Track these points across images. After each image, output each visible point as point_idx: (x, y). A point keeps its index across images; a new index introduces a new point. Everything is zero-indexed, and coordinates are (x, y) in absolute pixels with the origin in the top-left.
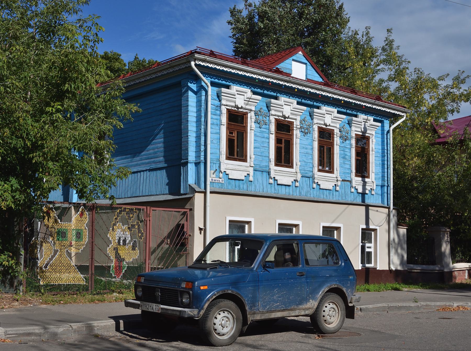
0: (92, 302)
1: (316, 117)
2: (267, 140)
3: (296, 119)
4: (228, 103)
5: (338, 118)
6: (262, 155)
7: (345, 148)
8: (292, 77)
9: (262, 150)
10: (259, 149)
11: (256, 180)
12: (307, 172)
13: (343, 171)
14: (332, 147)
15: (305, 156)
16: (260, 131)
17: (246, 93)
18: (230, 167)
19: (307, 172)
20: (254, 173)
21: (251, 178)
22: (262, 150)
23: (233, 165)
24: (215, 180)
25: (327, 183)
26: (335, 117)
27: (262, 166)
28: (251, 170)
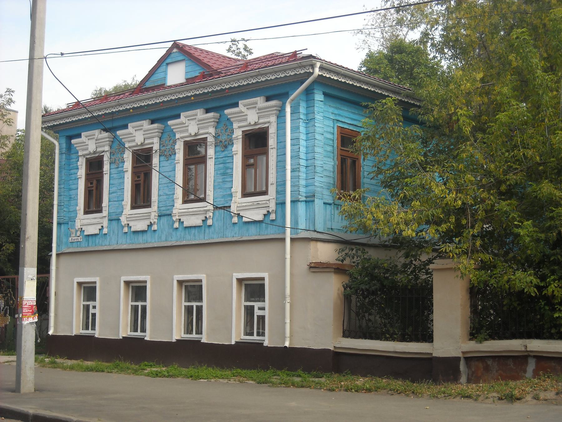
0: (72, 369)
1: (176, 130)
2: (112, 182)
3: (153, 143)
4: (182, 135)
5: (204, 120)
6: (119, 200)
7: (227, 158)
8: (170, 87)
9: (119, 194)
10: (115, 194)
11: (112, 231)
12: (169, 207)
13: (221, 193)
14: (340, 147)
15: (168, 186)
16: (118, 171)
17: (196, 115)
18: (85, 222)
19: (169, 207)
20: (109, 224)
21: (105, 231)
22: (119, 194)
23: (96, 219)
24: (74, 240)
25: (193, 218)
26: (201, 120)
27: (117, 213)
28: (105, 223)
